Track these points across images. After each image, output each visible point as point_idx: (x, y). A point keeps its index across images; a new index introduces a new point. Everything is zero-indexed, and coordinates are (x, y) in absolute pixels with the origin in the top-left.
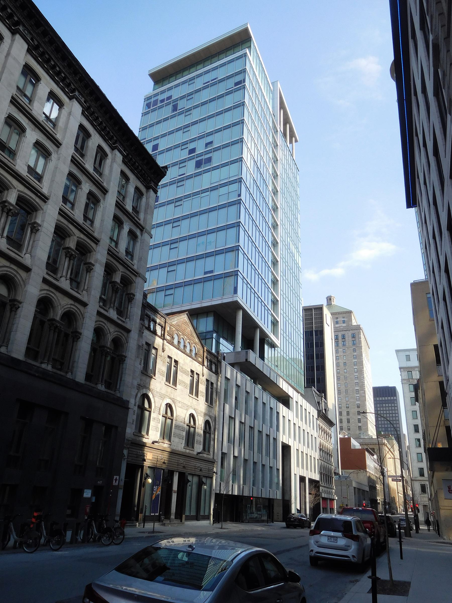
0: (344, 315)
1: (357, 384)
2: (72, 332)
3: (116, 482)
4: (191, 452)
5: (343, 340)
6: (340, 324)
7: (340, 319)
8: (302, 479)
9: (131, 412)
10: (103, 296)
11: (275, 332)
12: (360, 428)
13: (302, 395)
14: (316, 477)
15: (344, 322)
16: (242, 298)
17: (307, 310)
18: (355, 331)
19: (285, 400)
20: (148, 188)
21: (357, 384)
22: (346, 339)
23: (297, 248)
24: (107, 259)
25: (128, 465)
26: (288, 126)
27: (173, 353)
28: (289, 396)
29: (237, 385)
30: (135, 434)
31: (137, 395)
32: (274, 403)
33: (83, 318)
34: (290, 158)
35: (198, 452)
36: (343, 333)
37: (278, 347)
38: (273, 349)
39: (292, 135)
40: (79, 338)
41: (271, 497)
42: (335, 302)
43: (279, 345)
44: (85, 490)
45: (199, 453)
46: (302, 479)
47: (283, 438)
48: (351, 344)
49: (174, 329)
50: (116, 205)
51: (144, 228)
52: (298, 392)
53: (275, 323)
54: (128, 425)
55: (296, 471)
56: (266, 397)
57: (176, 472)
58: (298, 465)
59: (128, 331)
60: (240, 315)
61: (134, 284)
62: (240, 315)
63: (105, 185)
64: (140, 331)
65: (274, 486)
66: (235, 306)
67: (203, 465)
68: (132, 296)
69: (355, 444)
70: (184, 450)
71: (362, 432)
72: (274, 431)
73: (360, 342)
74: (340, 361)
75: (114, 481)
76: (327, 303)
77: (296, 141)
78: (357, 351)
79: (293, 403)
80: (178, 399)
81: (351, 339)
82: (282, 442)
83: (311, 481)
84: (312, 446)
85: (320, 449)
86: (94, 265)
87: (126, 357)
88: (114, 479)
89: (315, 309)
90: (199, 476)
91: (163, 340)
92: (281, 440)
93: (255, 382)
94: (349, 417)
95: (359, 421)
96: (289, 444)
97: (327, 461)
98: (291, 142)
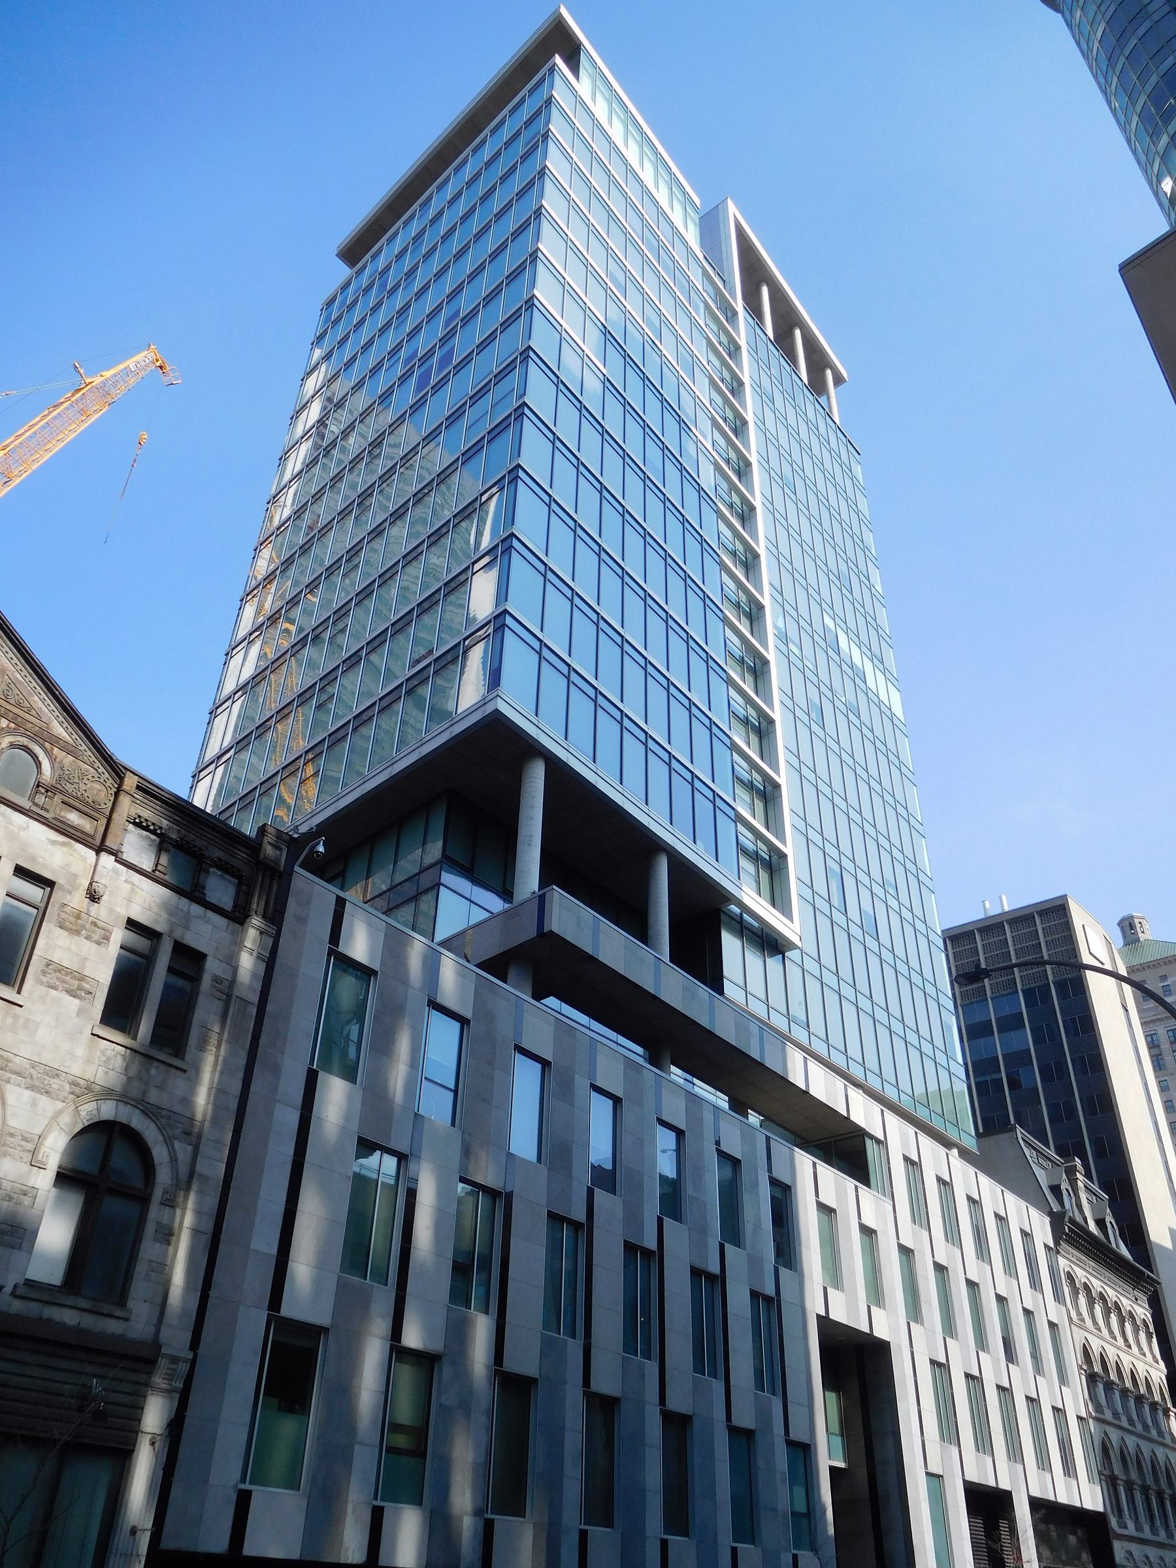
4: (113, 1327)
8: (988, 1506)
11: (778, 898)
13: (964, 1154)
14: (1088, 1495)
19: (847, 1150)
26: (765, 291)
28: (860, 1134)
37: (792, 946)
39: (818, 362)
42: (1147, 933)
43: (795, 939)
46: (988, 1506)
47: (830, 1295)
52: (947, 1144)
53: (772, 866)
55: (934, 1461)
56: (746, 1132)
58: (950, 1432)
60: (536, 779)
62: (536, 779)
65: (774, 1531)
72: (755, 1263)
76: (1124, 937)
77: (839, 380)
82: (824, 1322)
83: (1047, 1512)
84: (1036, 1355)
85: (1092, 1378)
91: (98, 852)
92: (815, 1306)
93: (655, 1059)
96: (878, 1333)
97: (1124, 1422)
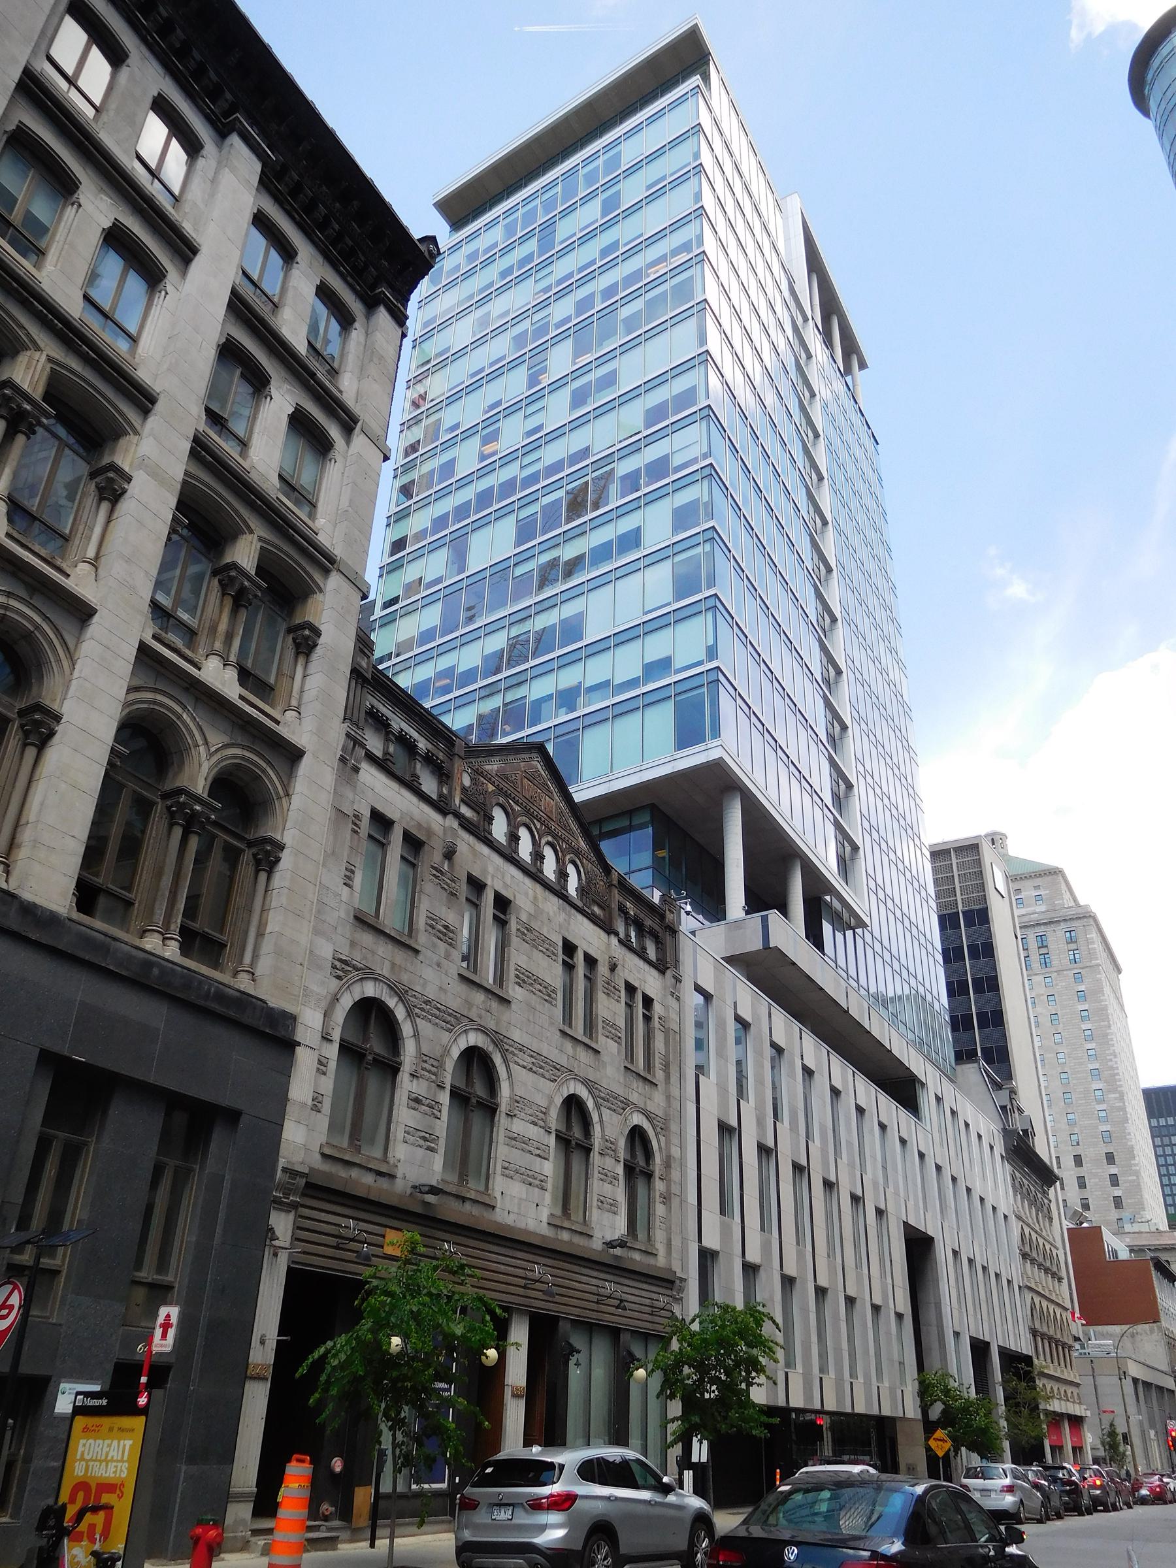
0: (1038, 882)
1: (1096, 1074)
2: (21, 713)
3: (164, 1336)
5: (1043, 951)
6: (1029, 906)
7: (1028, 893)
8: (980, 1349)
9: (305, 1060)
10: (161, 598)
12: (1118, 1203)
15: (1038, 898)
16: (733, 745)
17: (939, 854)
18: (1076, 923)
20: (371, 304)
21: (1096, 1074)
22: (1051, 947)
23: (893, 651)
24: (187, 473)
25: (296, 1279)
27: (491, 869)
29: (738, 1019)
30: (327, 1151)
31: (336, 999)
32: (868, 1094)
33: (73, 664)
34: (848, 404)
35: (609, 1238)
36: (1041, 930)
38: (849, 933)
40: (52, 734)
41: (886, 1412)
44: (62, 1386)
45: (611, 1245)
48: (1066, 962)
49: (491, 788)
50: (231, 306)
51: (356, 423)
54: (292, 1112)
57: (521, 1312)
59: (293, 755)
61: (318, 596)
63: (188, 227)
64: (343, 760)
66: (718, 782)
67: (635, 1294)
68: (307, 632)
69: (1118, 1246)
70: (545, 1230)
71: (1126, 1214)
73: (1092, 954)
74: (1039, 1009)
75: (158, 1332)
77: (863, 365)
78: (1086, 980)
79: (927, 1102)
80: (517, 1035)
81: (1064, 946)
86: (129, 479)
87: (281, 847)
88: (161, 1319)
89: (957, 850)
90: (614, 1333)
94: (1082, 1171)
95: (1114, 1181)
98: (848, 370)
